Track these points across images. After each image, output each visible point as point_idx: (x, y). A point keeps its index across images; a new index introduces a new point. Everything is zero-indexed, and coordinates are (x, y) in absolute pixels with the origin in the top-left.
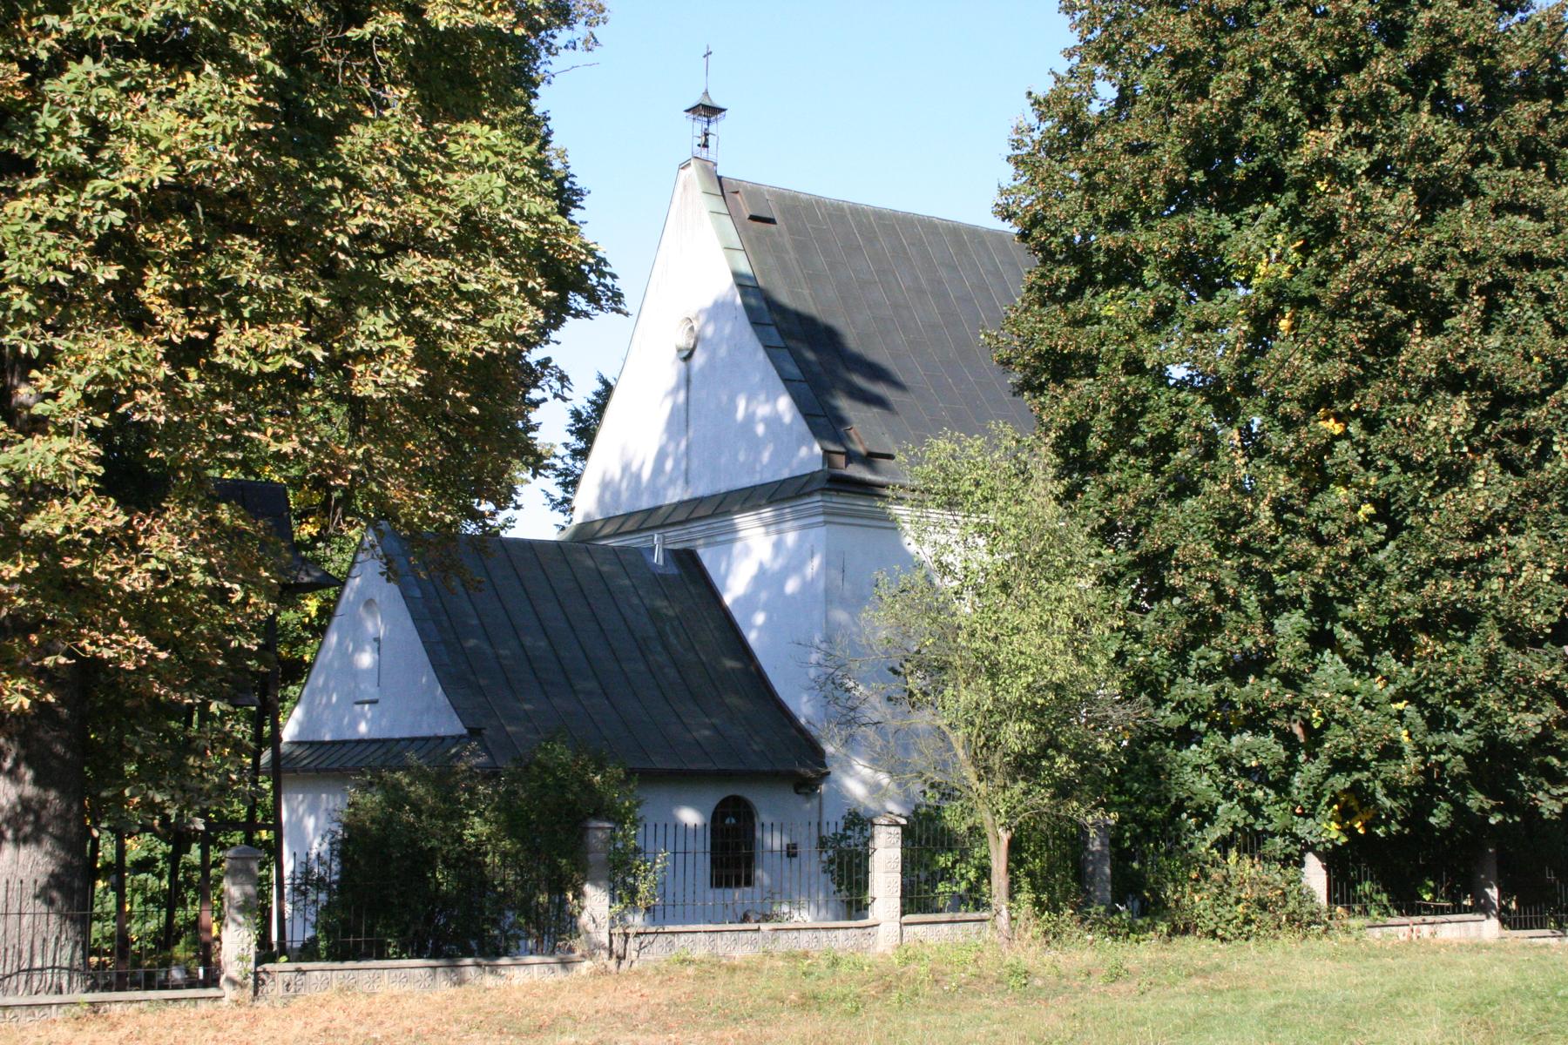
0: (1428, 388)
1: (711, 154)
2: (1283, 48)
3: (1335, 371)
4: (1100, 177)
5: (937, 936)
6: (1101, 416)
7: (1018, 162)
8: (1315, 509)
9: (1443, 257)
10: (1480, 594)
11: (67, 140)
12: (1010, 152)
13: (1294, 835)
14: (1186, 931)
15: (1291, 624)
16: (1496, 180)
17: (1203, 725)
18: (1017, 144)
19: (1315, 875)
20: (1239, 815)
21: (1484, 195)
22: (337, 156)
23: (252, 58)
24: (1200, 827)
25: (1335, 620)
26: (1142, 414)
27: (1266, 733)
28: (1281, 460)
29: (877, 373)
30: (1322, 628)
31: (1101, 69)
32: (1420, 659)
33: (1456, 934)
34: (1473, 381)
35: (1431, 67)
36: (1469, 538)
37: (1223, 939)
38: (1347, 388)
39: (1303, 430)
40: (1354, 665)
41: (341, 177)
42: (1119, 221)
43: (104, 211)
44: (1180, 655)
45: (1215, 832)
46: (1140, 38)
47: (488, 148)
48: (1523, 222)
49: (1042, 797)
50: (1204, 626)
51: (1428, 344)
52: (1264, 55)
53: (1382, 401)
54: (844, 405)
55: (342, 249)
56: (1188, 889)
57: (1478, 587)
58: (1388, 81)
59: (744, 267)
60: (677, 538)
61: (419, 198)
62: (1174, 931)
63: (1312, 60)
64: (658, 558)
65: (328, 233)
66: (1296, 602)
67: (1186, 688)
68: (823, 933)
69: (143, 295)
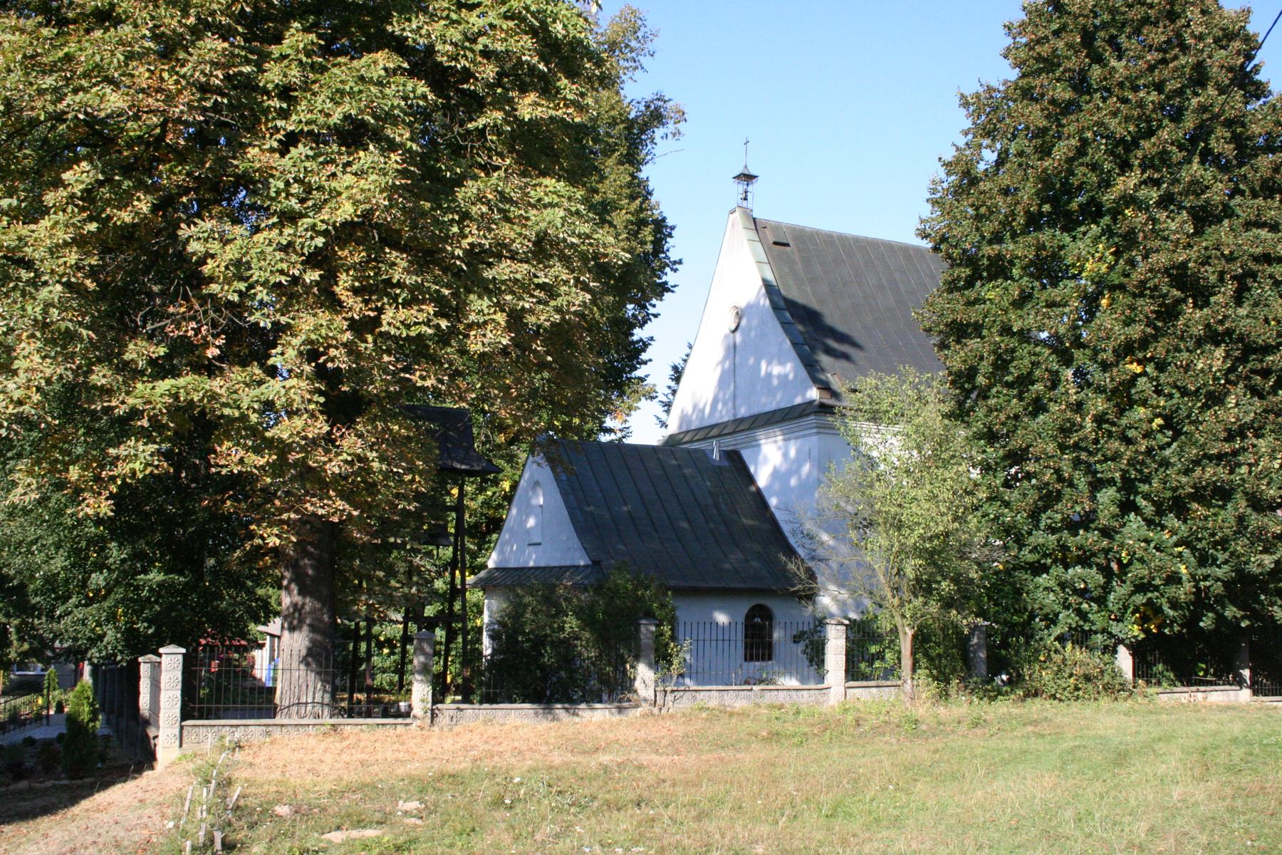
0: (1200, 342)
1: (749, 204)
2: (1100, 124)
3: (1136, 331)
4: (983, 210)
5: (867, 695)
6: (985, 363)
7: (935, 203)
8: (1124, 421)
9: (1210, 257)
10: (1232, 477)
11: (288, 195)
12: (928, 196)
13: (1110, 633)
14: (1036, 695)
15: (1107, 496)
16: (1245, 207)
17: (1049, 561)
18: (934, 191)
19: (1124, 660)
20: (1074, 620)
21: (1238, 216)
22: (455, 200)
23: (398, 139)
24: (1048, 627)
25: (1137, 493)
26: (1013, 360)
27: (1090, 567)
28: (1100, 390)
29: (843, 338)
30: (1128, 499)
31: (986, 142)
32: (1193, 519)
33: (1221, 698)
34: (1231, 339)
35: (1202, 132)
36: (1226, 440)
37: (1060, 700)
38: (1144, 343)
39: (1115, 370)
40: (1149, 523)
41: (457, 213)
42: (997, 238)
43: (312, 238)
44: (1034, 515)
45: (1057, 631)
46: (1008, 121)
47: (555, 193)
48: (1264, 233)
49: (934, 607)
50: (1049, 499)
51: (1198, 314)
52: (1088, 129)
53: (1168, 351)
54: (825, 360)
55: (458, 258)
56: (1037, 668)
57: (1232, 472)
58: (1172, 144)
59: (770, 277)
60: (729, 443)
61: (508, 225)
62: (1027, 695)
63: (1120, 131)
64: (716, 455)
65: (449, 248)
66: (1111, 482)
67: (1039, 538)
68: (794, 693)
69: (337, 289)
